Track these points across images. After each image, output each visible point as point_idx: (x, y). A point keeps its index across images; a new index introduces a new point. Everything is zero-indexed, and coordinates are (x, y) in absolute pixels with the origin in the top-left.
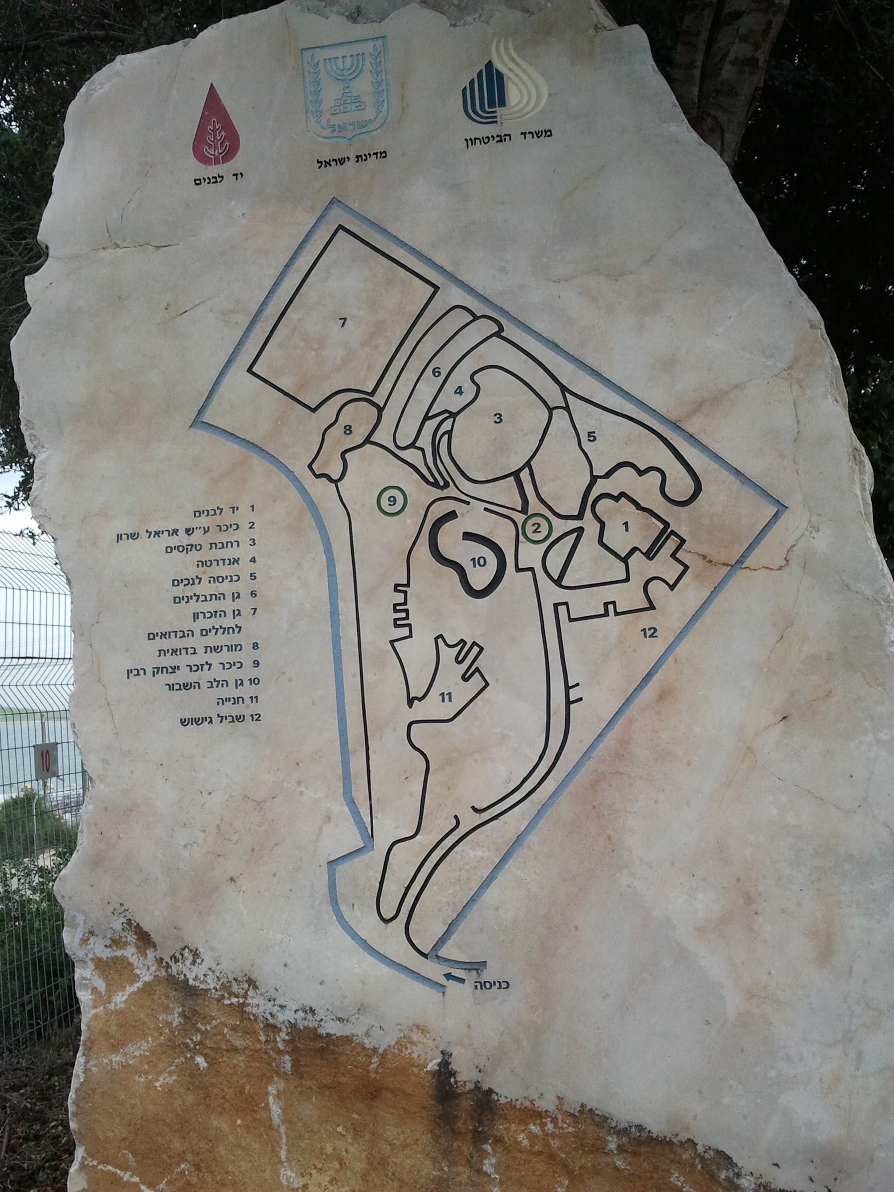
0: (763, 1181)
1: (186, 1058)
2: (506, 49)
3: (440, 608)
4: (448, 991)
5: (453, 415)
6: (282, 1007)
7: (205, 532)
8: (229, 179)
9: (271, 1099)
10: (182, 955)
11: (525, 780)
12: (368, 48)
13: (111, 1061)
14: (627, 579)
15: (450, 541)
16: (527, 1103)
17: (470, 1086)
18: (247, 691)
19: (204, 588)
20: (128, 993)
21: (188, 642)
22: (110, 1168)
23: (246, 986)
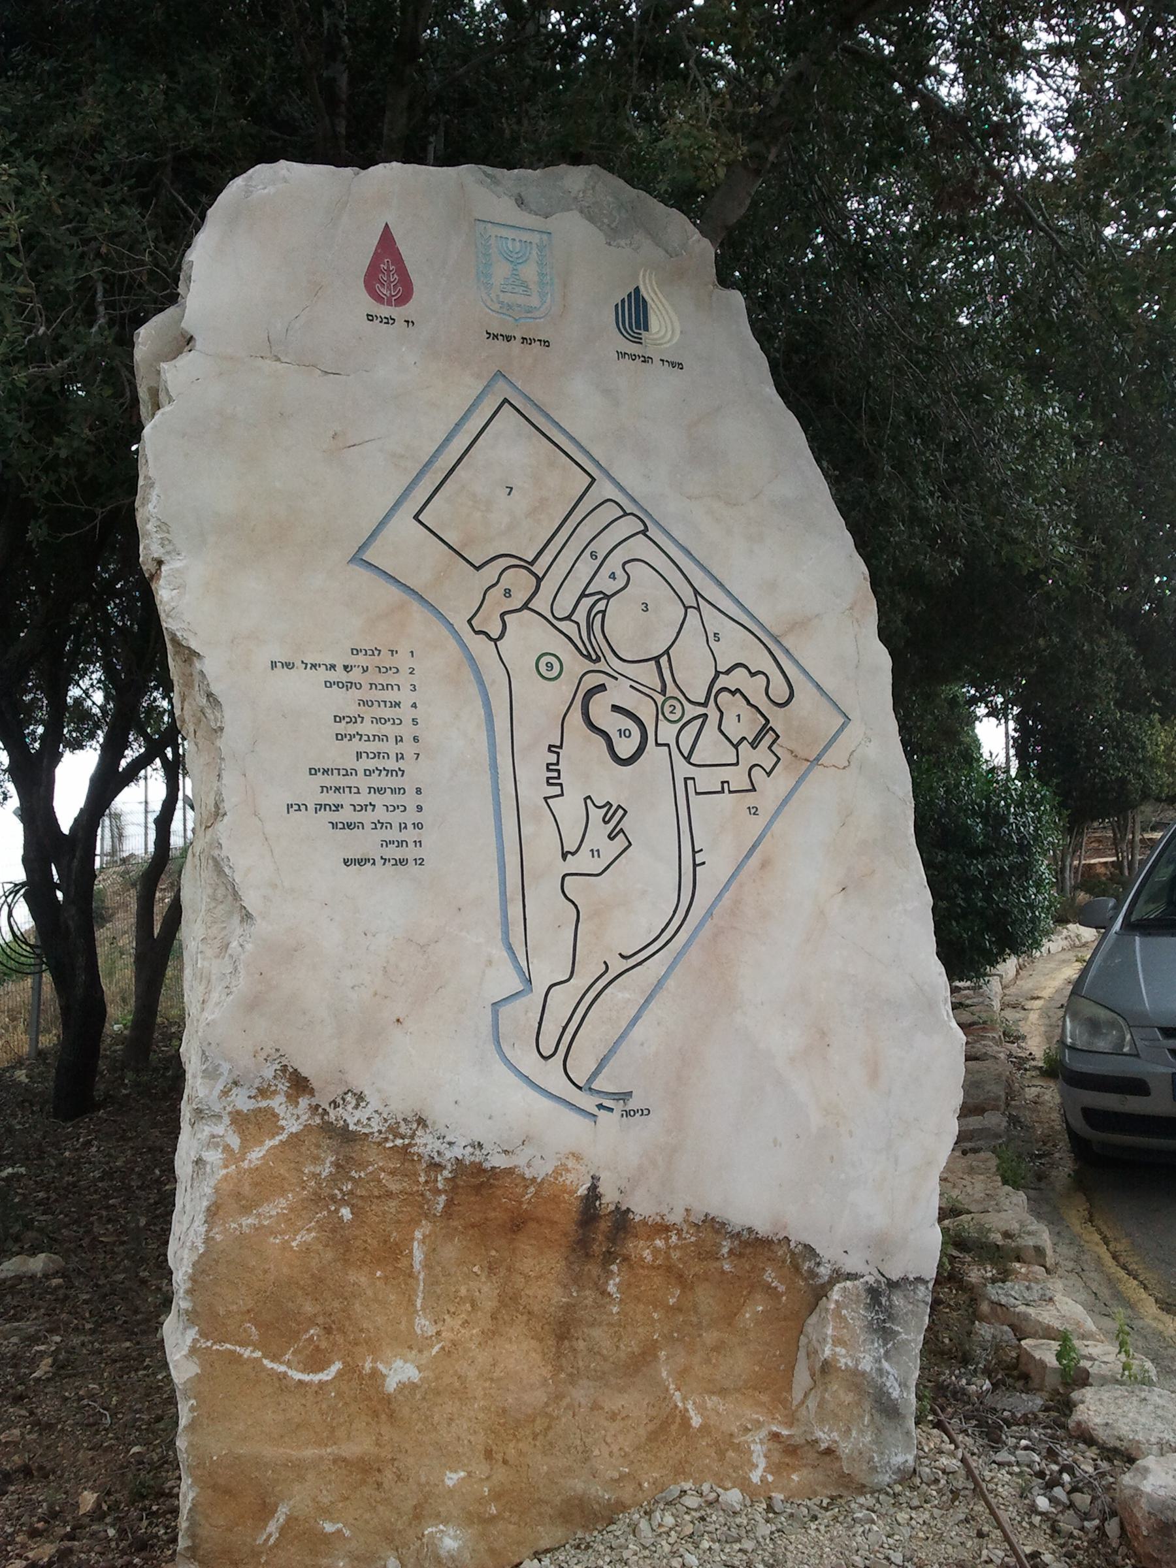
0: (836, 1267)
1: (329, 1211)
2: (650, 277)
3: (590, 773)
4: (599, 1120)
5: (608, 597)
6: (450, 1144)
7: (364, 671)
8: (400, 323)
9: (416, 1244)
10: (344, 1100)
11: (663, 931)
12: (536, 238)
13: (241, 1225)
14: (737, 764)
15: (600, 709)
16: (658, 1219)
17: (612, 1207)
18: (410, 835)
19: (367, 728)
20: (266, 1148)
21: (351, 781)
22: (229, 1346)
23: (415, 1126)
